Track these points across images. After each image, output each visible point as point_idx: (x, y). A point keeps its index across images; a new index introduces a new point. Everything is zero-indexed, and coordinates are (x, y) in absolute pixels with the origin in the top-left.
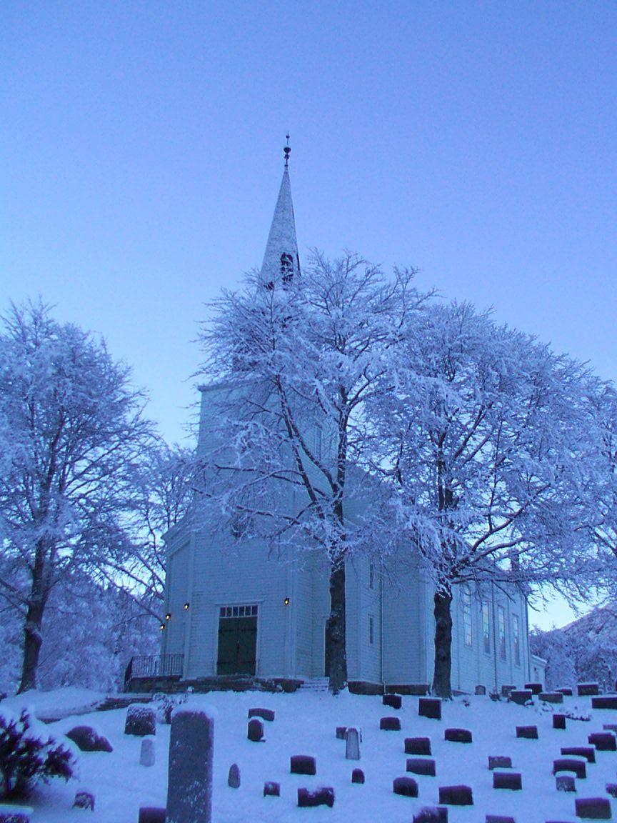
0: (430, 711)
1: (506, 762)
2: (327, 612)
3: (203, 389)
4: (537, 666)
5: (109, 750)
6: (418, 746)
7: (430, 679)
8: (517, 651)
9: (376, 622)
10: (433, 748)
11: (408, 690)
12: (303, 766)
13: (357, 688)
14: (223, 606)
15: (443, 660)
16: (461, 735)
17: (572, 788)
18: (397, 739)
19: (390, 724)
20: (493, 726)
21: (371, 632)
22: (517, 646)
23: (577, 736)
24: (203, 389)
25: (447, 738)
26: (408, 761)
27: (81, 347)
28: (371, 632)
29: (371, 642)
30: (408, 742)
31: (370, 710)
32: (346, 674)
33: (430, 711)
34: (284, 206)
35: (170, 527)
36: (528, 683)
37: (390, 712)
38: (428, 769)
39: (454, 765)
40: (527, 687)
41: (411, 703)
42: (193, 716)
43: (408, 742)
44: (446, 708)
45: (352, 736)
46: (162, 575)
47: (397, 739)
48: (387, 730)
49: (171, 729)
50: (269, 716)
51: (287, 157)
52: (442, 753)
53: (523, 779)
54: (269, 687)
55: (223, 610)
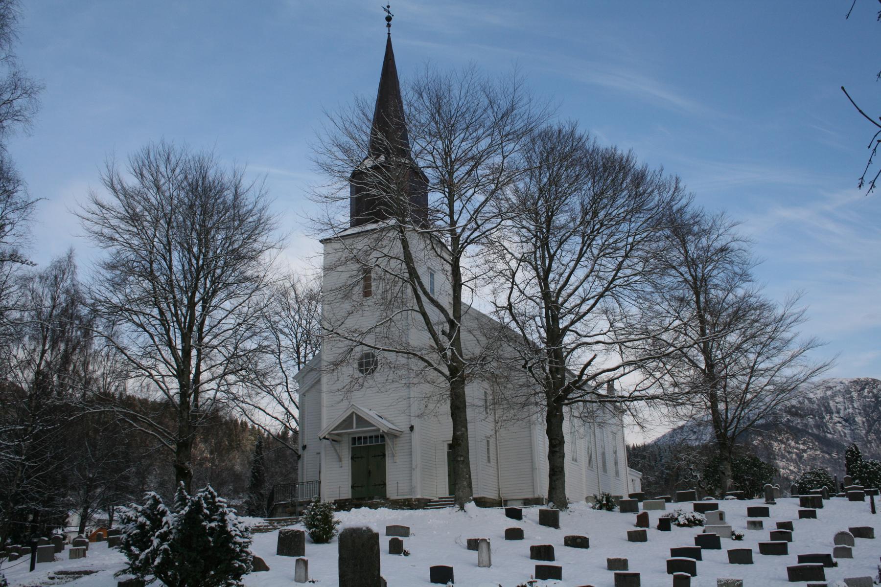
0: (549, 520)
3: (324, 241)
4: (634, 478)
6: (542, 552)
7: (544, 493)
9: (492, 441)
10: (556, 554)
11: (528, 502)
13: (482, 503)
15: (556, 473)
16: (579, 540)
18: (523, 547)
19: (514, 534)
21: (488, 453)
22: (604, 454)
24: (324, 241)
25: (566, 544)
26: (537, 567)
27: (751, 308)
28: (488, 453)
29: (489, 461)
30: (533, 548)
31: (496, 521)
33: (549, 520)
36: (631, 492)
37: (513, 524)
40: (631, 496)
43: (533, 548)
44: (563, 516)
45: (483, 546)
46: (296, 413)
47: (523, 547)
48: (740, 563)
51: (389, 26)
53: (563, 571)
54: (397, 505)
55: (354, 439)
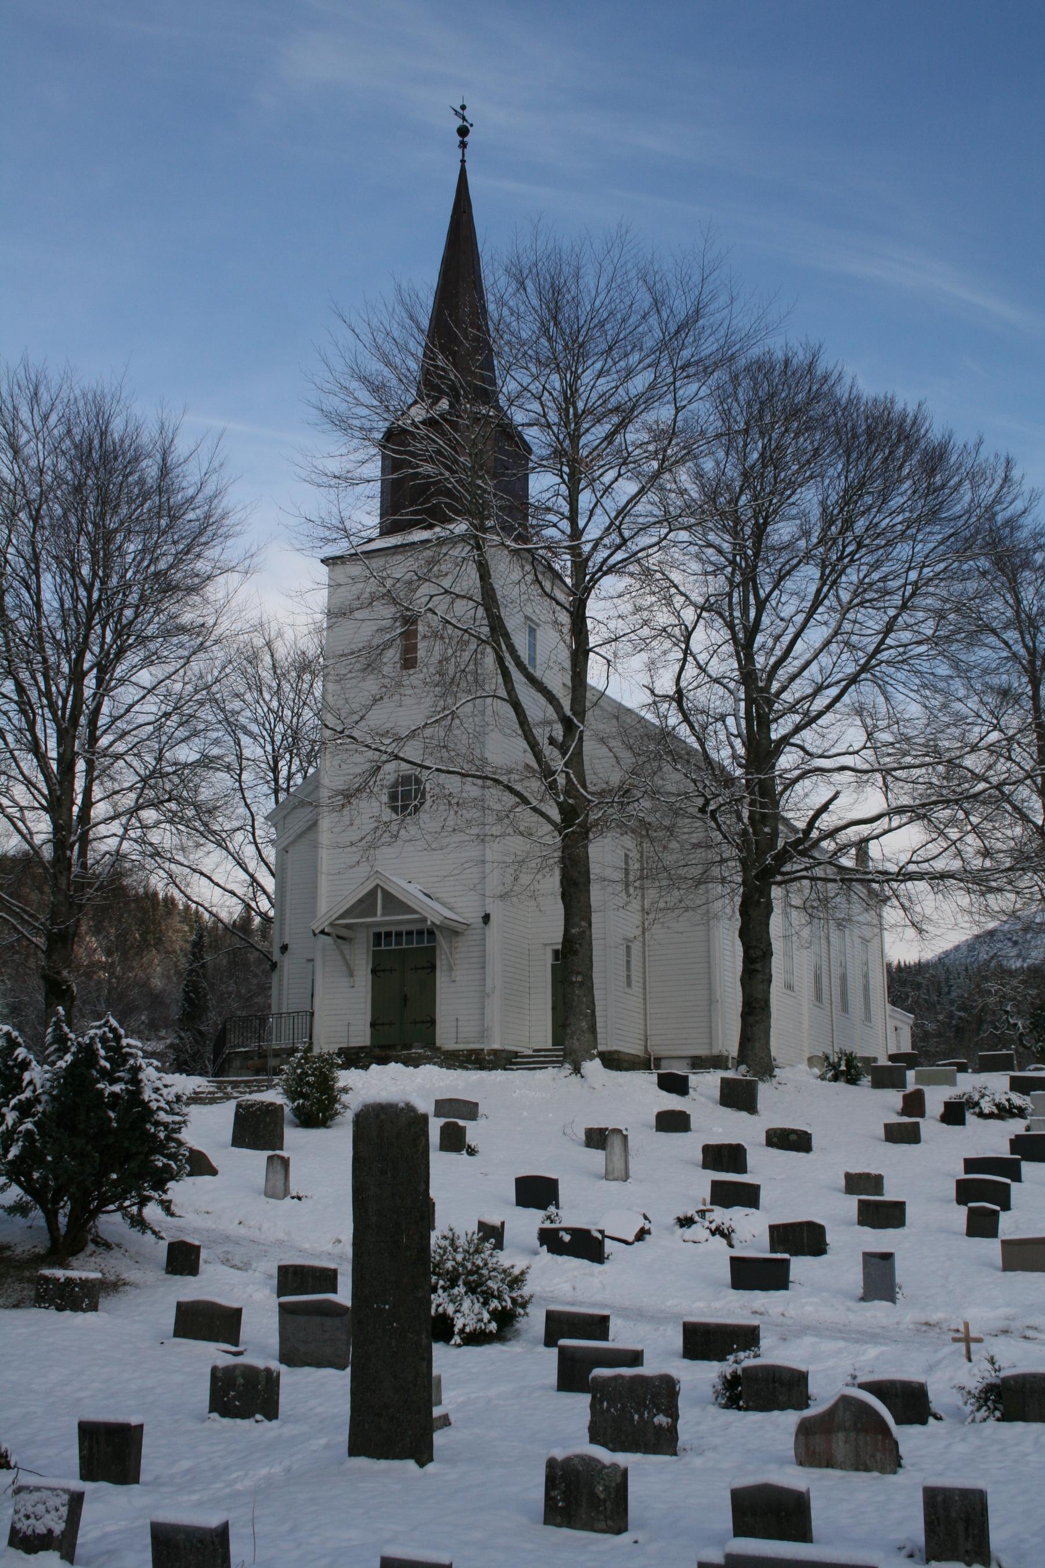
0: (739, 1097)
1: (875, 1183)
2: (552, 927)
5: (213, 1172)
6: (725, 1157)
8: (866, 988)
11: (699, 1063)
12: (537, 1192)
13: (613, 1061)
14: (377, 930)
15: (755, 1010)
16: (793, 1137)
17: (991, 1231)
19: (672, 1122)
20: (851, 1125)
23: (993, 1139)
26: (715, 1184)
28: (628, 969)
29: (629, 984)
30: (707, 1149)
31: (639, 1097)
32: (595, 1038)
33: (739, 1097)
34: (463, 161)
35: (281, 800)
36: (893, 1051)
37: (672, 1102)
38: (747, 1196)
39: (792, 1189)
40: (892, 1058)
41: (707, 1084)
42: (661, 1420)
43: (707, 1149)
45: (616, 1142)
46: (269, 883)
49: (592, 1406)
50: (471, 1110)
52: (764, 1166)
55: (377, 936)
